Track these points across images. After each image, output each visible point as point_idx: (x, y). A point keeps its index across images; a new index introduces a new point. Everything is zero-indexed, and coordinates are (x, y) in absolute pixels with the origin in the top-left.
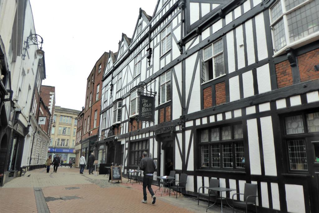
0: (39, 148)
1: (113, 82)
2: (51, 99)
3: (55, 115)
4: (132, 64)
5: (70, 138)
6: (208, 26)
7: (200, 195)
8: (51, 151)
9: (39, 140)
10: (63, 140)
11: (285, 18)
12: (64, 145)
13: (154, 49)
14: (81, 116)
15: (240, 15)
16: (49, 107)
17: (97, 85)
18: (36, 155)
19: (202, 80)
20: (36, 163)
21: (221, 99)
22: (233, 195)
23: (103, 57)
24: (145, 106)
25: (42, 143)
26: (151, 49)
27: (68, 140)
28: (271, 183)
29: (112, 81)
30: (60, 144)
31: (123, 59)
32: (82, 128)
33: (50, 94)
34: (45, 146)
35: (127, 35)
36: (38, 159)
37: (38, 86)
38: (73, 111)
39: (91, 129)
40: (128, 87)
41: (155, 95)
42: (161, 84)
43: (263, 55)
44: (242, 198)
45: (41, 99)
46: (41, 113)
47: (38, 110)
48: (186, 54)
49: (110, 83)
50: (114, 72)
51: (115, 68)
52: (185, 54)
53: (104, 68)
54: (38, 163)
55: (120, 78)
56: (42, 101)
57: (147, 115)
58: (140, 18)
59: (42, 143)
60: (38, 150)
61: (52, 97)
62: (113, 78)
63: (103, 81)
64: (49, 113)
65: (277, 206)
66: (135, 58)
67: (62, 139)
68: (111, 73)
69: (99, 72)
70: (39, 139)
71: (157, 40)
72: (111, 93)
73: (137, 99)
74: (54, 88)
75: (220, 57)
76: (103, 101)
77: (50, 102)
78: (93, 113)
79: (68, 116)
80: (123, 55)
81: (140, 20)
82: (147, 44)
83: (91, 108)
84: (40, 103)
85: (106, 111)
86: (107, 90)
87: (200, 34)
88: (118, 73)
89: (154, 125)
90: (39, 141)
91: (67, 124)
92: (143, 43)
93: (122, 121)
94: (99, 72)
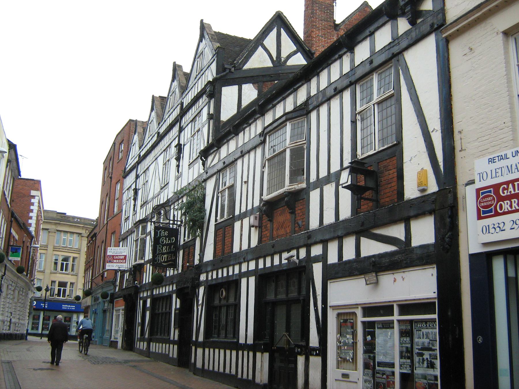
0: (11, 301)
1: (138, 184)
2: (33, 204)
3: (43, 229)
5: (77, 279)
6: (279, 99)
7: (208, 371)
9: (10, 287)
10: (63, 284)
11: (227, 190)
14: (92, 238)
15: (316, 93)
16: (30, 221)
18: (6, 314)
19: (216, 220)
20: (6, 330)
21: (499, 164)
22: (141, 348)
23: (126, 127)
24: (163, 242)
25: (17, 292)
26: (181, 144)
27: (72, 284)
28: (257, 353)
31: (152, 146)
32: (93, 264)
33: (32, 194)
34: (23, 298)
35: (211, 25)
36: (10, 322)
37: (7, 197)
38: (83, 221)
40: (154, 200)
42: (359, 109)
43: (347, 160)
44: (144, 349)
45: (13, 215)
46: (14, 237)
47: (8, 231)
49: (176, 142)
50: (140, 165)
51: (141, 159)
53: (128, 150)
54: (9, 330)
55: (196, 129)
56: (16, 219)
58: (201, 40)
59: (17, 292)
60: (10, 306)
61: (35, 201)
62: (137, 177)
63: (125, 177)
64: (29, 233)
65: (250, 377)
67: (59, 283)
68: (135, 167)
69: (120, 157)
70: (11, 285)
71: (187, 133)
72: (178, 166)
73: (288, 153)
74: (39, 182)
75: (388, 103)
77: (32, 211)
79: (73, 233)
80: (130, 164)
81: (202, 45)
82: (174, 137)
83: (106, 227)
84: (11, 221)
85: (128, 236)
86: (169, 161)
87: (351, 49)
88: (191, 119)
89: (178, 272)
90: (10, 289)
91: (71, 250)
93: (145, 260)
94: (120, 157)
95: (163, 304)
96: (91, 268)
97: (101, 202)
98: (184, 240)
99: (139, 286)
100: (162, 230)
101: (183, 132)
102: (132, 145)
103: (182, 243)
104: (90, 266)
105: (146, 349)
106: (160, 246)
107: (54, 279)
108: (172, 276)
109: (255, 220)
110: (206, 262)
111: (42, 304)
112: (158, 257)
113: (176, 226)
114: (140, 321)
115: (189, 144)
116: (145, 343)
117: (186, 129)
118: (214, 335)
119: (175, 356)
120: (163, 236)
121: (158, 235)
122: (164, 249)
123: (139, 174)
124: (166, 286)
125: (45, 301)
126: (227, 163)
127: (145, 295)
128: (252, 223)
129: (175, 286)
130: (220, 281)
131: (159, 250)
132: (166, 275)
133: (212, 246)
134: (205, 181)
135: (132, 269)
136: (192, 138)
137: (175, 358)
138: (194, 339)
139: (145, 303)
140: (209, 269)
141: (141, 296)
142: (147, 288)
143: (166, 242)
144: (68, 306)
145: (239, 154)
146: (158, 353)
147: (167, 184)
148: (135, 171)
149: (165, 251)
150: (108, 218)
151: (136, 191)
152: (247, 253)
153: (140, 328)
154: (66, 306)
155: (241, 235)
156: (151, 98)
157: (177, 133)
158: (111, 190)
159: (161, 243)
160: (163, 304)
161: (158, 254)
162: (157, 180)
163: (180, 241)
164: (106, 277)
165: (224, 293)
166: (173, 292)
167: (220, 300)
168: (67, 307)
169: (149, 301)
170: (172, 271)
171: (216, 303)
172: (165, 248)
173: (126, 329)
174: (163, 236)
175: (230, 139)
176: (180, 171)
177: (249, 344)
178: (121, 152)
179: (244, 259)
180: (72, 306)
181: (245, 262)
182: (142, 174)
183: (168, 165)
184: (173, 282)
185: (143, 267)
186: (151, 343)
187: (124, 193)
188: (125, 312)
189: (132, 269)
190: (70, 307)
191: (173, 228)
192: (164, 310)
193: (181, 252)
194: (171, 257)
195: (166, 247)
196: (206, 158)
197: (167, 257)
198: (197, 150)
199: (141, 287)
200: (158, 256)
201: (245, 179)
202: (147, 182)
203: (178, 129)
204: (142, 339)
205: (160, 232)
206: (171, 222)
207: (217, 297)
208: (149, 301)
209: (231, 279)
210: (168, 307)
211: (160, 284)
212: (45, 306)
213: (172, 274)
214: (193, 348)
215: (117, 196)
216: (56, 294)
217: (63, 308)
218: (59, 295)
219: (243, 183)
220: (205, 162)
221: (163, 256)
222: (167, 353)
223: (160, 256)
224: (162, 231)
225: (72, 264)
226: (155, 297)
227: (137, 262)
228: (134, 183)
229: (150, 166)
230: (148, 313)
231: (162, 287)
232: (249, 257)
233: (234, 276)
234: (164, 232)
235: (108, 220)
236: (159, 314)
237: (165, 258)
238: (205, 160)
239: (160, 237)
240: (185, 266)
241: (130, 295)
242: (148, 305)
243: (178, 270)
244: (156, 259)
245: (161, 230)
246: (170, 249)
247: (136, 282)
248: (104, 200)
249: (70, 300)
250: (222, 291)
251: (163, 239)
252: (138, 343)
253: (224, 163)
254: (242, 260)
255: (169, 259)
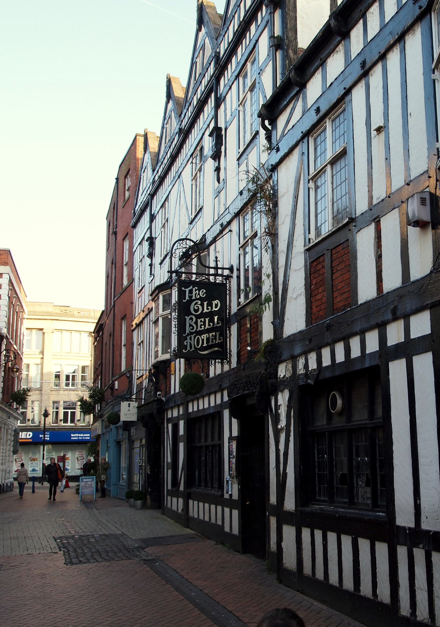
4: (187, 175)
7: (313, 579)
8: (36, 441)
12: (73, 421)
13: (226, 129)
17: (124, 239)
22: (174, 508)
26: (220, 128)
29: (150, 228)
30: (61, 416)
32: (101, 372)
39: (116, 376)
41: (228, 277)
48: (143, 311)
50: (155, 197)
52: (142, 312)
57: (205, 345)
62: (152, 218)
66: (237, 76)
68: (148, 204)
72: (218, 169)
76: (137, 289)
78: (117, 323)
92: (239, 50)
95: (213, 427)
96: (100, 377)
97: (107, 276)
98: (239, 304)
99: (164, 399)
100: (193, 287)
101: (222, 106)
102: (143, 171)
103: (234, 309)
104: (97, 375)
105: (182, 510)
106: (191, 319)
107: (56, 399)
108: (219, 375)
109: (422, 206)
110: (289, 337)
111: (41, 436)
112: (188, 340)
113: (220, 278)
114: (169, 460)
115: (235, 121)
116: (181, 500)
117: (228, 97)
118: (320, 496)
119: (236, 531)
120: (197, 299)
121: (187, 298)
122: (199, 324)
123: (154, 214)
124: (209, 395)
125: (45, 430)
126: (323, 110)
127: (175, 414)
128: (414, 215)
129: (225, 393)
130: (328, 375)
131: (190, 325)
132: (208, 376)
133: (302, 301)
134: (274, 168)
135: (153, 371)
136: (241, 108)
137: (234, 536)
138: (273, 499)
139: (176, 428)
140: (298, 350)
141: (168, 417)
142: (179, 403)
143: (203, 310)
144: (80, 435)
145: (357, 71)
146: (204, 522)
147: (201, 209)
148: (148, 210)
149: (203, 326)
150: (114, 297)
151: (151, 241)
152: (401, 297)
153: (170, 471)
154: (77, 435)
155: (379, 258)
156: (165, 80)
157: (213, 113)
158: (117, 252)
159: (193, 312)
160: (213, 427)
161: (188, 335)
162: (184, 210)
163: (230, 307)
164: (117, 390)
165: (339, 402)
166: (223, 405)
167: (330, 416)
168: (78, 437)
169: (182, 424)
170: (219, 366)
171: (318, 424)
172: (201, 321)
173: (149, 473)
174: (197, 299)
175: (328, 56)
176: (222, 178)
177: (428, 532)
178: (128, 190)
179: (394, 312)
180: (86, 435)
181: (395, 319)
182: (158, 212)
183: (200, 177)
184: (223, 387)
185: (169, 366)
186: (191, 502)
187: (135, 251)
188: (83, 471)
189: (153, 371)
190: (82, 437)
191: (215, 282)
192: (209, 439)
193: (234, 328)
194: (205, 325)
195: (203, 320)
196: (273, 122)
197: (208, 339)
198: (251, 125)
199: (168, 401)
200: (188, 338)
201: (378, 120)
202: (167, 221)
203: (213, 105)
204: (175, 493)
205: (191, 292)
206: (212, 271)
207: (322, 410)
208: (182, 424)
209: (358, 367)
210: (216, 435)
211: (194, 394)
212: (44, 437)
213: (219, 371)
214: (273, 521)
215: (126, 258)
216: (61, 420)
217: (72, 438)
218: (65, 420)
219: (374, 133)
220: (271, 133)
221: (198, 338)
222: (219, 522)
223: (193, 336)
224: (194, 289)
225: (82, 376)
226: (193, 416)
227: (159, 359)
228: (148, 230)
229: (170, 192)
230: (181, 446)
231: (203, 397)
232: (409, 305)
233: (367, 358)
234: (197, 292)
235: (115, 299)
236: (201, 447)
237: (203, 340)
238: (270, 127)
239: (191, 301)
240: (242, 353)
241: (151, 415)
242: (181, 432)
243: (229, 362)
244: (186, 344)
245: (191, 288)
246: (211, 324)
247: (158, 393)
248: (110, 271)
249: (81, 426)
250: (334, 397)
251: (196, 303)
252: (169, 498)
253: (318, 110)
254: (389, 316)
255: (210, 343)
